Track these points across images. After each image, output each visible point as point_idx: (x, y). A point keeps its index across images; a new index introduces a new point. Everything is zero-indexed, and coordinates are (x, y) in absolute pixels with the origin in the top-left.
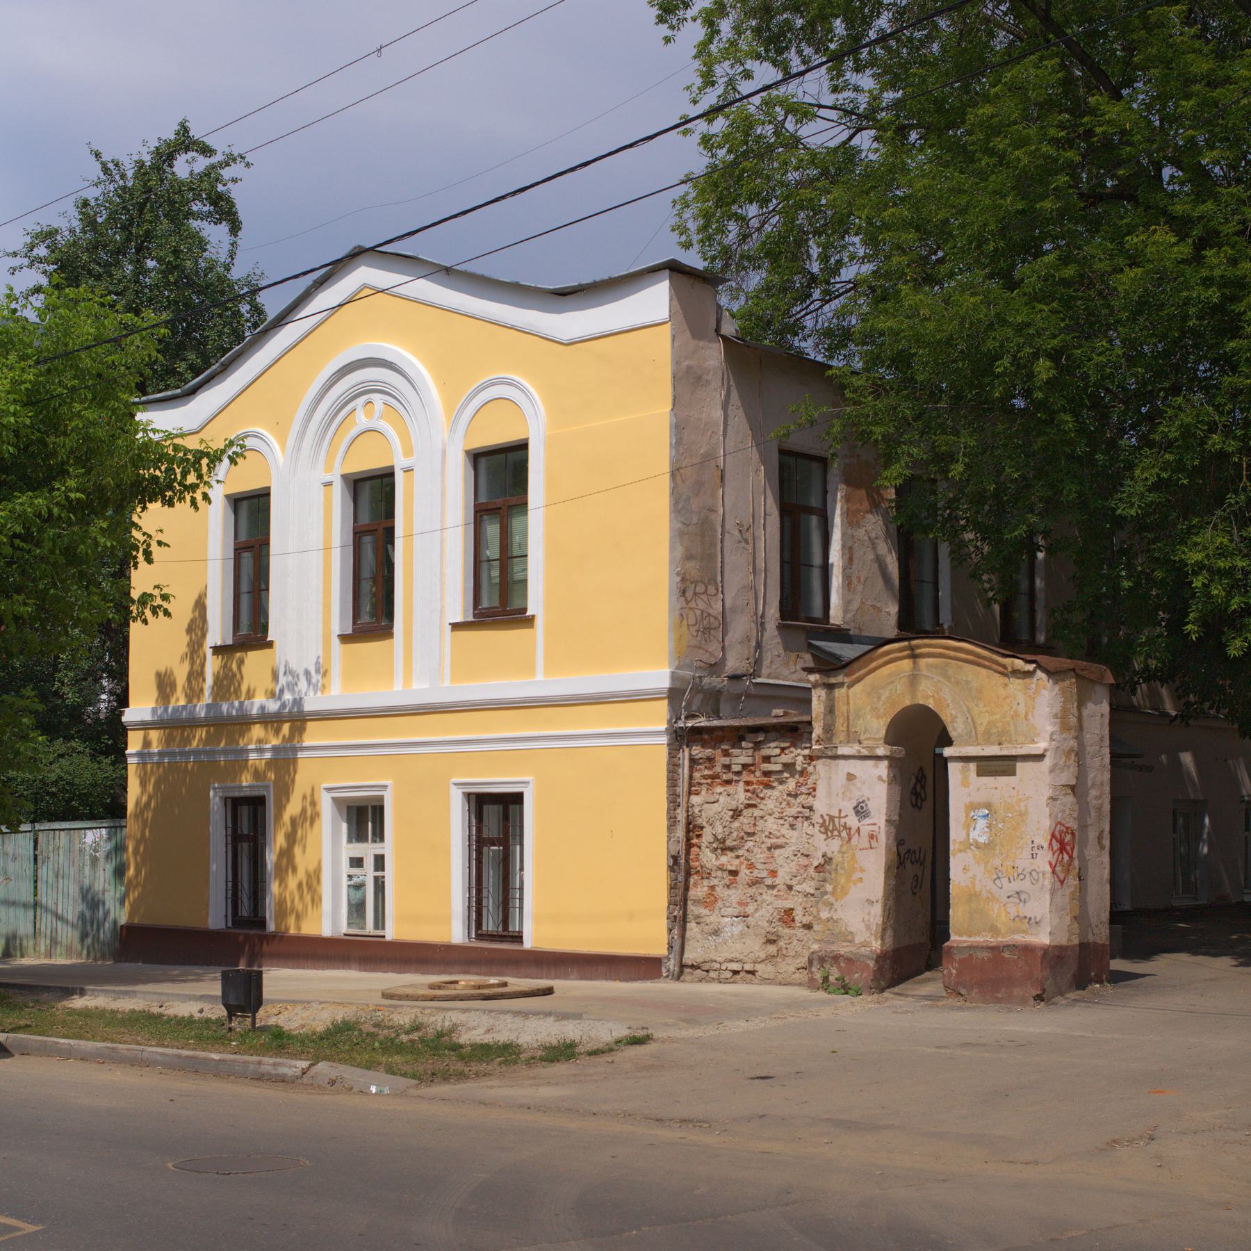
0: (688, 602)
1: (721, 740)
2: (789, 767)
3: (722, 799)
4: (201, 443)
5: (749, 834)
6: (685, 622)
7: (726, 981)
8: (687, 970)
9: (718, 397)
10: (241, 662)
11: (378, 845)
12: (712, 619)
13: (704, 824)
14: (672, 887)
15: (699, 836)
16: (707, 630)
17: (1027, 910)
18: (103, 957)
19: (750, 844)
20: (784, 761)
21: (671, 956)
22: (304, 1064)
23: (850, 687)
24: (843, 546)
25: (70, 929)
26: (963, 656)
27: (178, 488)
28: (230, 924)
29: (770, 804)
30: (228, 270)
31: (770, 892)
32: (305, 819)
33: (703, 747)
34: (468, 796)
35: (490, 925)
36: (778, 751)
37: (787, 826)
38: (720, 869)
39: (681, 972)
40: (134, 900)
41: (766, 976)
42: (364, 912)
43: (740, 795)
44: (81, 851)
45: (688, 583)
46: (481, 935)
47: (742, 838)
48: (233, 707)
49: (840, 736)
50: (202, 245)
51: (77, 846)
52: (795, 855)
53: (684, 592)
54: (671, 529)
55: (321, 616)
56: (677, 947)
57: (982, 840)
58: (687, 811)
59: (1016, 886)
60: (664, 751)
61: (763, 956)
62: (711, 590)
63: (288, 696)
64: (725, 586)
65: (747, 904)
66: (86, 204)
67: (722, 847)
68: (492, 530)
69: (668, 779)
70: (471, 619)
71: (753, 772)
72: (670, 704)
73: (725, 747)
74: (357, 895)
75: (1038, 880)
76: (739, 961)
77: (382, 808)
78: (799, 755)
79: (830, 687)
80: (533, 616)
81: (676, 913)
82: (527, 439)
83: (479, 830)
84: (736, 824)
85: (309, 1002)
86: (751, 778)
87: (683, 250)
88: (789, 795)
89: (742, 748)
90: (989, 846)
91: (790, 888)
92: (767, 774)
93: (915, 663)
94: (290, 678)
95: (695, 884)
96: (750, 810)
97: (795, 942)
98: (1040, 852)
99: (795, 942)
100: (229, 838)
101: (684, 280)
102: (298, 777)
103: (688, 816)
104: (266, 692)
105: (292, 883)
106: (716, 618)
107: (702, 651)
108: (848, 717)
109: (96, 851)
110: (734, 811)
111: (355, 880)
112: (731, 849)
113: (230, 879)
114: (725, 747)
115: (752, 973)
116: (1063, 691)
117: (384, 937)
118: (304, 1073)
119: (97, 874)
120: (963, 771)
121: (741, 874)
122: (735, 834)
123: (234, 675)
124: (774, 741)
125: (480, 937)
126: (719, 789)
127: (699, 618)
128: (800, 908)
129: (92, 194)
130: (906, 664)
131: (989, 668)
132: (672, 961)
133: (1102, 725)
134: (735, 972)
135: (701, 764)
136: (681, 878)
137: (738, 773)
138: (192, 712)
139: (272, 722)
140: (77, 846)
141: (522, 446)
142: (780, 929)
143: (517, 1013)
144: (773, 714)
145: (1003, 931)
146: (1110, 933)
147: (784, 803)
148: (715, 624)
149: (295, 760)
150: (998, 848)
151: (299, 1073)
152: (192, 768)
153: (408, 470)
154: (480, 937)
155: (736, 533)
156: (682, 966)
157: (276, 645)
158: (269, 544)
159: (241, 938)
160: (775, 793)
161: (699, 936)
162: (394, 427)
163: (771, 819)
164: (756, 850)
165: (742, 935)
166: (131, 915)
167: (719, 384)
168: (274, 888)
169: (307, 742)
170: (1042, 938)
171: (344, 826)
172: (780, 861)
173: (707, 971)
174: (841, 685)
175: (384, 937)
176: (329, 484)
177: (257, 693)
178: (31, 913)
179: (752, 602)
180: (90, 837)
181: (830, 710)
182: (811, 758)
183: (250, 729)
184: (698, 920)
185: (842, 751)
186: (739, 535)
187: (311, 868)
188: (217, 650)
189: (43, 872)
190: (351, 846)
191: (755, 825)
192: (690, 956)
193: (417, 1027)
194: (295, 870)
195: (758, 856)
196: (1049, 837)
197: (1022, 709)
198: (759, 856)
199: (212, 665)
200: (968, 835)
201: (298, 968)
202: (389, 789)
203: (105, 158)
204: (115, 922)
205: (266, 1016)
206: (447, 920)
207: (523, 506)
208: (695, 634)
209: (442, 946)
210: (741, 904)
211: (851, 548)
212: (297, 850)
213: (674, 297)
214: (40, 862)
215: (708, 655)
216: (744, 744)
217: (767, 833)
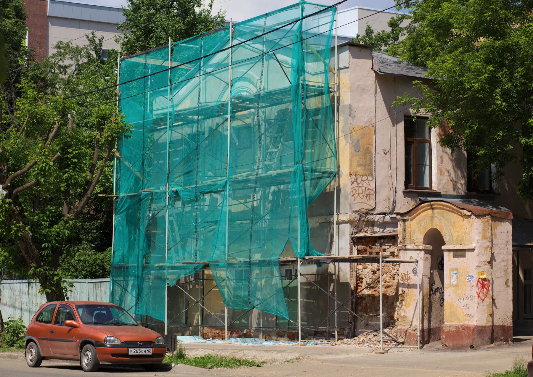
13: (363, 277)
15: (362, 282)
17: (469, 312)
23: (411, 220)
24: (438, 156)
26: (448, 209)
36: (388, 247)
49: (408, 241)
57: (455, 283)
58: (357, 272)
59: (466, 302)
75: (472, 299)
79: (404, 221)
90: (457, 286)
93: (433, 211)
98: (473, 288)
103: (357, 274)
107: (365, 204)
108: (411, 233)
110: (373, 272)
116: (483, 223)
120: (449, 255)
127: (364, 191)
130: (430, 211)
131: (457, 214)
133: (507, 236)
145: (462, 320)
146: (513, 321)
148: (372, 192)
150: (460, 286)
170: (474, 322)
174: (408, 220)
181: (405, 230)
182: (399, 250)
185: (408, 247)
196: (477, 282)
197: (467, 230)
200: (450, 281)
208: (362, 197)
211: (442, 157)
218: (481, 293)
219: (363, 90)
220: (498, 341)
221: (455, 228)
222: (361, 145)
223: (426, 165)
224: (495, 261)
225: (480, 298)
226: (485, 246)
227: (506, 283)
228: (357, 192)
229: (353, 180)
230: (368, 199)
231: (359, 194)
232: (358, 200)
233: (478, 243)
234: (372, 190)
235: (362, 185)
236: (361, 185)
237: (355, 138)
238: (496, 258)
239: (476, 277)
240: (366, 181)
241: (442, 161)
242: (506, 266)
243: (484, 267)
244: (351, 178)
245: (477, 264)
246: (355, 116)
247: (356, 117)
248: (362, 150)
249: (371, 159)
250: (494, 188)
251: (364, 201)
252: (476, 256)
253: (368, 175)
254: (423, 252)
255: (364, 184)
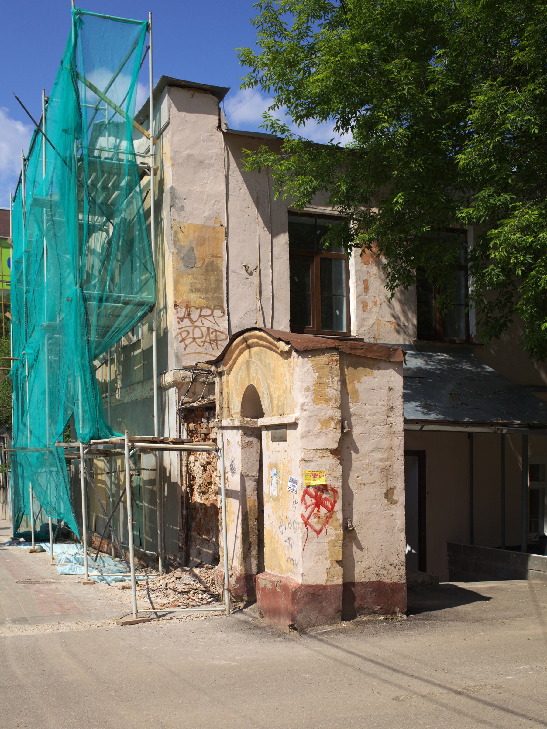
23: (228, 374)
116: (318, 368)
127: (205, 334)
133: (390, 398)
211: (366, 282)
218: (312, 517)
219: (201, 164)
220: (366, 614)
221: (275, 383)
222: (197, 256)
223: (344, 296)
224: (357, 451)
225: (311, 527)
226: (323, 418)
227: (389, 495)
228: (191, 335)
229: (181, 315)
230: (216, 348)
231: (194, 339)
232: (194, 347)
233: (303, 409)
234: (222, 333)
235: (200, 324)
236: (199, 323)
237: (183, 244)
238: (358, 444)
239: (301, 483)
240: (211, 318)
241: (366, 289)
242: (388, 459)
243: (320, 461)
244: (177, 312)
245: (301, 455)
246: (183, 206)
247: (185, 209)
248: (199, 264)
249: (219, 281)
250: (473, 336)
251: (205, 351)
252: (299, 438)
253: (212, 307)
254: (240, 432)
255: (205, 321)
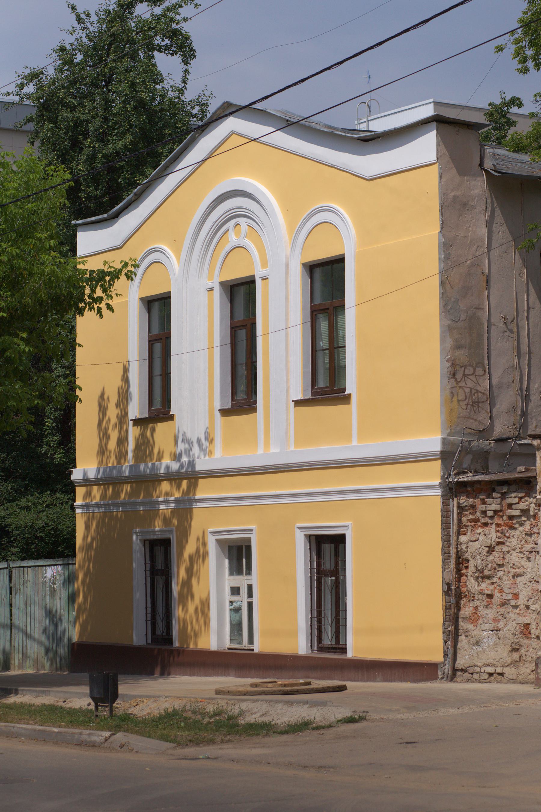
0: (457, 382)
1: (480, 491)
2: (525, 512)
3: (481, 538)
4: (105, 264)
5: (500, 566)
6: (455, 399)
7: (484, 681)
8: (459, 673)
9: (484, 217)
10: (153, 430)
11: (248, 577)
12: (480, 395)
13: (470, 558)
14: (447, 608)
15: (467, 567)
16: (476, 404)
18: (61, 669)
19: (500, 573)
20: (522, 508)
21: (447, 662)
22: (107, 734)
25: (36, 646)
27: (88, 300)
28: (149, 641)
29: (513, 542)
30: (183, 94)
31: (515, 611)
32: (199, 556)
33: (467, 497)
34: (309, 537)
35: (327, 641)
36: (516, 500)
37: (525, 559)
38: (481, 593)
39: (454, 675)
40: (83, 621)
41: (511, 677)
42: (241, 630)
43: (493, 534)
44: (43, 583)
45: (457, 367)
46: (321, 648)
47: (495, 569)
48: (148, 467)
50: (157, 78)
51: (41, 580)
52: (531, 582)
53: (454, 375)
54: (441, 326)
55: (207, 394)
56: (450, 656)
60: (439, 501)
61: (509, 661)
62: (479, 371)
63: (185, 459)
64: (492, 366)
65: (499, 621)
66: (62, 49)
67: (481, 576)
68: (324, 325)
69: (442, 523)
70: (309, 396)
71: (502, 517)
72: (443, 463)
73: (482, 497)
74: (236, 617)
76: (493, 665)
77: (249, 548)
78: (532, 503)
80: (350, 395)
81: (450, 629)
82: (344, 255)
83: (319, 565)
84: (491, 558)
85: (159, 697)
86: (500, 521)
87: (522, 74)
88: (526, 534)
89: (493, 498)
91: (528, 607)
92: (511, 518)
94: (187, 446)
95: (465, 606)
96: (500, 547)
97: (531, 650)
99: (531, 650)
100: (148, 572)
101: (450, 130)
102: (193, 523)
104: (171, 454)
105: (191, 608)
106: (484, 394)
107: (471, 421)
109: (54, 583)
110: (489, 547)
111: (235, 605)
112: (488, 577)
113: (149, 605)
114: (482, 497)
115: (502, 674)
117: (253, 650)
118: (106, 740)
119: (55, 602)
121: (495, 597)
122: (490, 566)
123: (149, 441)
124: (514, 492)
125: (321, 649)
126: (479, 530)
127: (468, 395)
128: (535, 623)
129: (69, 40)
132: (447, 667)
134: (491, 674)
135: (467, 510)
136: (453, 599)
137: (492, 518)
138: (120, 471)
139: (175, 480)
140: (41, 580)
141: (340, 261)
142: (521, 640)
143: (266, 701)
144: (518, 471)
147: (524, 541)
149: (191, 509)
151: (103, 740)
152: (121, 516)
153: (264, 279)
154: (321, 649)
155: (502, 325)
156: (455, 670)
157: (176, 418)
158: (170, 337)
159: (156, 652)
160: (517, 533)
161: (467, 646)
162: (255, 244)
163: (514, 554)
164: (505, 578)
165: (495, 644)
166: (81, 634)
167: (484, 207)
168: (178, 612)
169: (198, 496)
171: (227, 561)
172: (521, 586)
173: (472, 674)
175: (253, 650)
176: (211, 290)
177: (165, 455)
178: (8, 632)
179: (517, 379)
180: (49, 572)
183: (160, 484)
184: (467, 634)
186: (504, 326)
187: (204, 596)
188: (137, 422)
189: (18, 600)
190: (232, 577)
191: (503, 558)
192: (461, 662)
193: (218, 713)
194: (192, 597)
195: (506, 583)
198: (507, 583)
199: (133, 432)
201: (194, 675)
202: (254, 532)
203: (80, 10)
204: (70, 640)
205: (120, 705)
206: (294, 634)
207: (341, 307)
208: (465, 407)
209: (291, 656)
210: (495, 620)
212: (194, 581)
213: (441, 143)
214: (13, 593)
215: (477, 423)
216: (494, 494)
217: (511, 565)
